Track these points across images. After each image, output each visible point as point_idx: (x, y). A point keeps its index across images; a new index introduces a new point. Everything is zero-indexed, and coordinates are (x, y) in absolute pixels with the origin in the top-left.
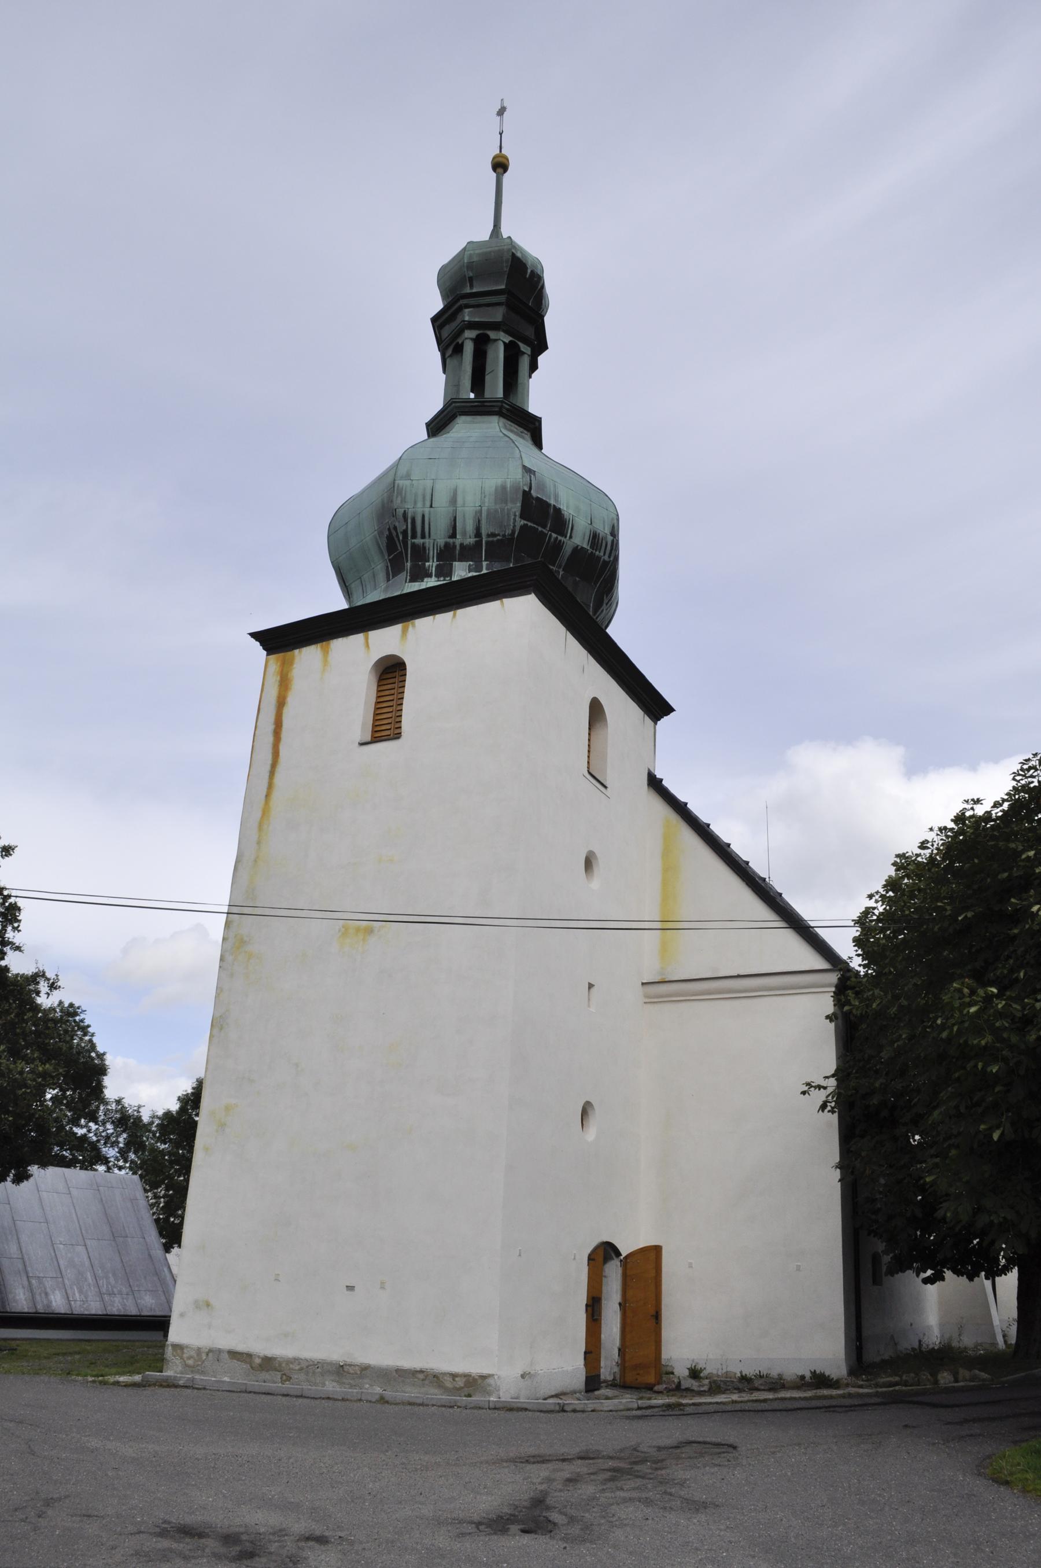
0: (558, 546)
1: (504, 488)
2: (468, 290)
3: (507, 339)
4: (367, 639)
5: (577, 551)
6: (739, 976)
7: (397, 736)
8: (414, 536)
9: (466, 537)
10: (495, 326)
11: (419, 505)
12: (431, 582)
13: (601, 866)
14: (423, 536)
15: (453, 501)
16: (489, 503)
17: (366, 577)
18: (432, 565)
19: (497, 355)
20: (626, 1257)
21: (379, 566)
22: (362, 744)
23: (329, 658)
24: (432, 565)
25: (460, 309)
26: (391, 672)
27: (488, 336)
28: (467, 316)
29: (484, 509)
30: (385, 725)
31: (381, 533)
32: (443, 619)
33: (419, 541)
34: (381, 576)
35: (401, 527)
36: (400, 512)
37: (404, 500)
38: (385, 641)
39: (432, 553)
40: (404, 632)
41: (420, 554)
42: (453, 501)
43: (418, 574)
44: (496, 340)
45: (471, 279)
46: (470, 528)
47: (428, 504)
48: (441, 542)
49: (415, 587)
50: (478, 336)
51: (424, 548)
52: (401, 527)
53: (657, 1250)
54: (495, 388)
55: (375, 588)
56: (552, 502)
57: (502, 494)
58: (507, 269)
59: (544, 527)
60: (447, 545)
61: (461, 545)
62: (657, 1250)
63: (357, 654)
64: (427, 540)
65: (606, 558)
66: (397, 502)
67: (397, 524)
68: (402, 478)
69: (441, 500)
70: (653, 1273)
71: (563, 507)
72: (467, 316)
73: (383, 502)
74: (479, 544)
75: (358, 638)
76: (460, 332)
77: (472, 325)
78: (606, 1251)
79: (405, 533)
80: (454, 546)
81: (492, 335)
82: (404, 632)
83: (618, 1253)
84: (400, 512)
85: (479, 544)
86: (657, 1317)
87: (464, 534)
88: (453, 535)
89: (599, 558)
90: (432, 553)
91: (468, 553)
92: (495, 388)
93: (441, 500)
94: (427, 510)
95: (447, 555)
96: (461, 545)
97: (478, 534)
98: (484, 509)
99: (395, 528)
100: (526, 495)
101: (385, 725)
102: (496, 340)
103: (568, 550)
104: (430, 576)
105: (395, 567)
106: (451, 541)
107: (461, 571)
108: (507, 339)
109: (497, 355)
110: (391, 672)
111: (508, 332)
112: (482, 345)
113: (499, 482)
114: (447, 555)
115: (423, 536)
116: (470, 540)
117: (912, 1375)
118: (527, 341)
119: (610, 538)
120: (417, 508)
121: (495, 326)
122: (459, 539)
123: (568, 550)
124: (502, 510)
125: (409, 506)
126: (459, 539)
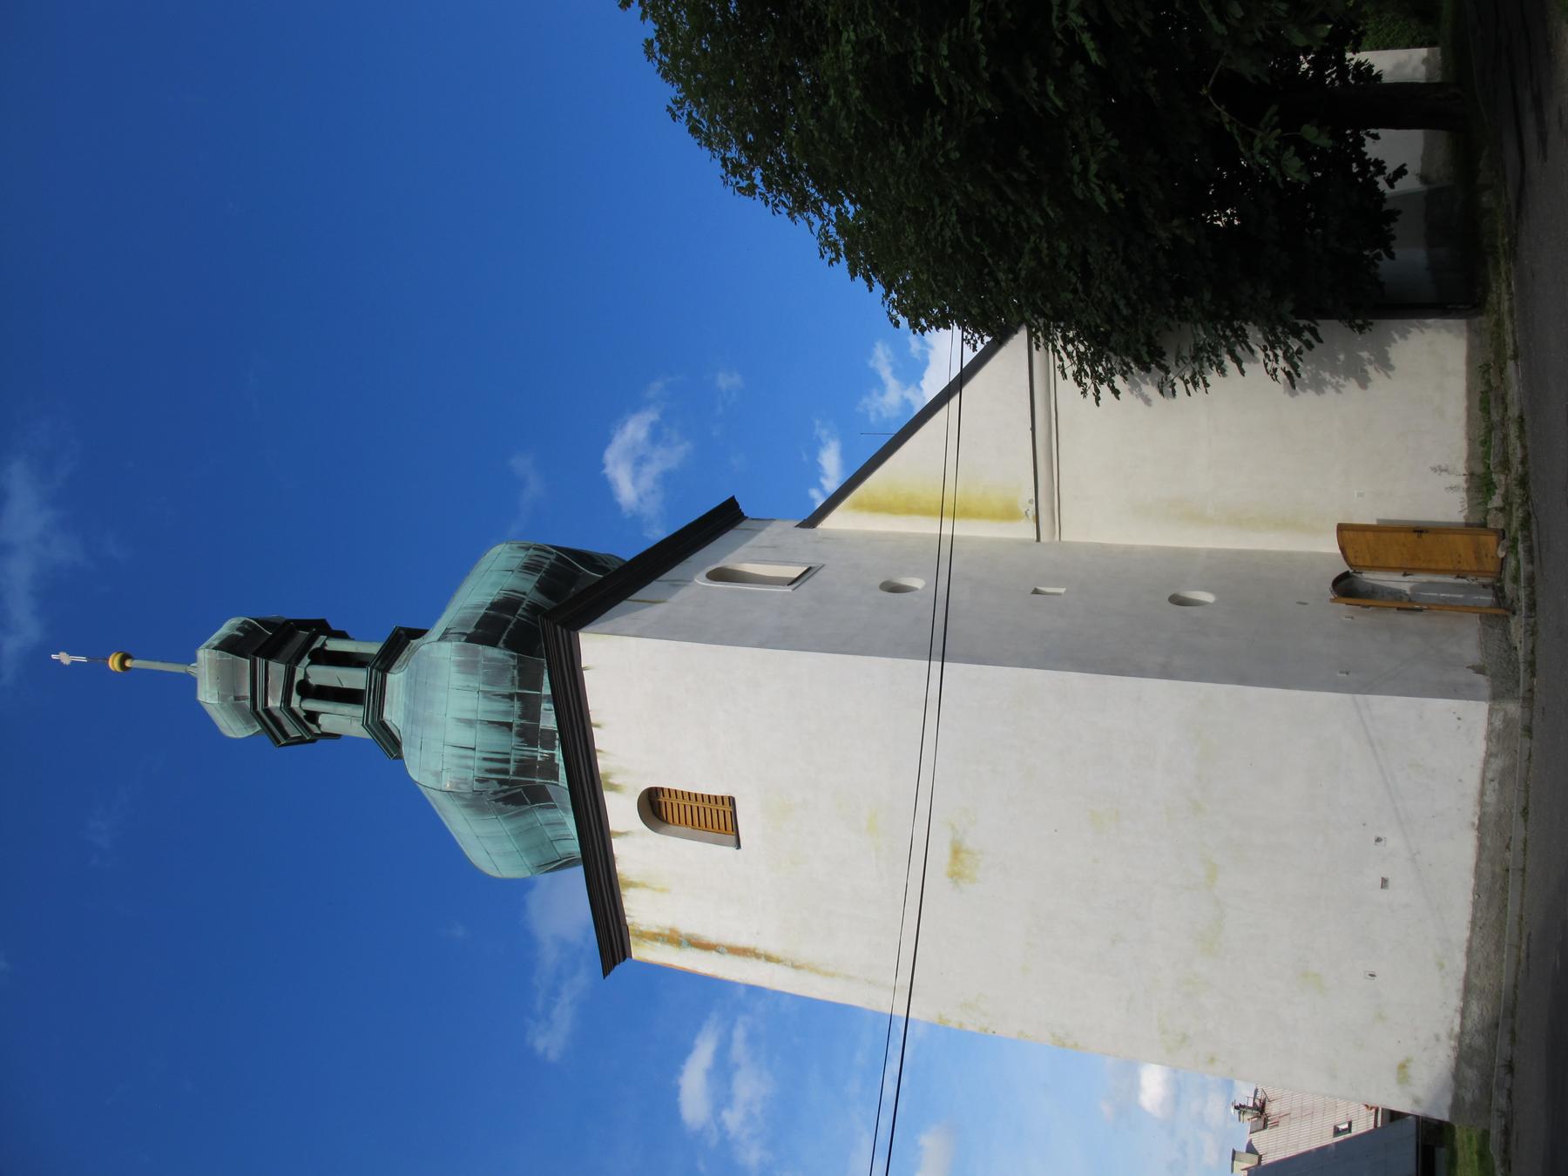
0: (534, 609)
1: (459, 664)
2: (248, 703)
3: (306, 660)
4: (619, 834)
5: (542, 587)
6: (1033, 429)
7: (732, 801)
8: (506, 772)
9: (512, 712)
10: (290, 674)
11: (470, 763)
12: (558, 754)
13: (1380, 835)
14: (507, 761)
15: (470, 723)
16: (476, 682)
17: (549, 832)
18: (541, 753)
19: (322, 675)
20: (1351, 566)
21: (541, 816)
22: (738, 846)
23: (635, 880)
24: (541, 753)
25: (268, 711)
26: (655, 807)
27: (301, 682)
28: (274, 703)
29: (482, 688)
30: (716, 818)
31: (500, 812)
32: (600, 739)
33: (512, 767)
34: (550, 815)
35: (495, 786)
36: (477, 786)
37: (465, 781)
38: (621, 811)
39: (527, 752)
40: (614, 788)
41: (526, 767)
42: (470, 723)
43: (549, 770)
44: (306, 675)
45: (237, 698)
46: (501, 706)
47: (470, 753)
48: (515, 741)
49: (562, 773)
50: (299, 693)
51: (521, 761)
52: (495, 786)
53: (1342, 529)
54: (355, 678)
55: (564, 824)
56: (483, 611)
57: (468, 667)
58: (231, 657)
59: (509, 622)
60: (520, 734)
61: (521, 717)
62: (1342, 529)
63: (635, 849)
64: (512, 757)
65: (552, 557)
66: (464, 788)
67: (491, 791)
68: (439, 781)
69: (467, 737)
70: (1369, 535)
71: (489, 600)
72: (274, 703)
73: (467, 806)
74: (521, 697)
75: (618, 846)
76: (292, 712)
77: (287, 699)
78: (1345, 587)
79: (501, 782)
80: (522, 725)
81: (299, 677)
82: (614, 788)
83: (1345, 575)
84: (477, 786)
85: (521, 697)
86: (1419, 530)
87: (507, 713)
88: (509, 726)
89: (552, 565)
90: (527, 752)
91: (530, 710)
92: (355, 678)
93: (467, 737)
94: (478, 755)
95: (530, 735)
96: (521, 717)
97: (510, 697)
98: (482, 688)
99: (495, 793)
100: (471, 639)
101: (716, 818)
102: (306, 675)
103: (539, 598)
104: (553, 756)
105: (538, 796)
106: (515, 729)
107: (548, 721)
108: (306, 660)
109: (322, 675)
110: (655, 807)
111: (298, 660)
112: (307, 691)
113: (454, 669)
114: (530, 735)
115: (507, 761)
116: (517, 704)
117: (956, 155)
118: (313, 639)
119: (531, 552)
120: (474, 766)
121: (290, 674)
122: (515, 720)
123: (539, 598)
124: (485, 667)
125: (470, 775)
126: (515, 720)
